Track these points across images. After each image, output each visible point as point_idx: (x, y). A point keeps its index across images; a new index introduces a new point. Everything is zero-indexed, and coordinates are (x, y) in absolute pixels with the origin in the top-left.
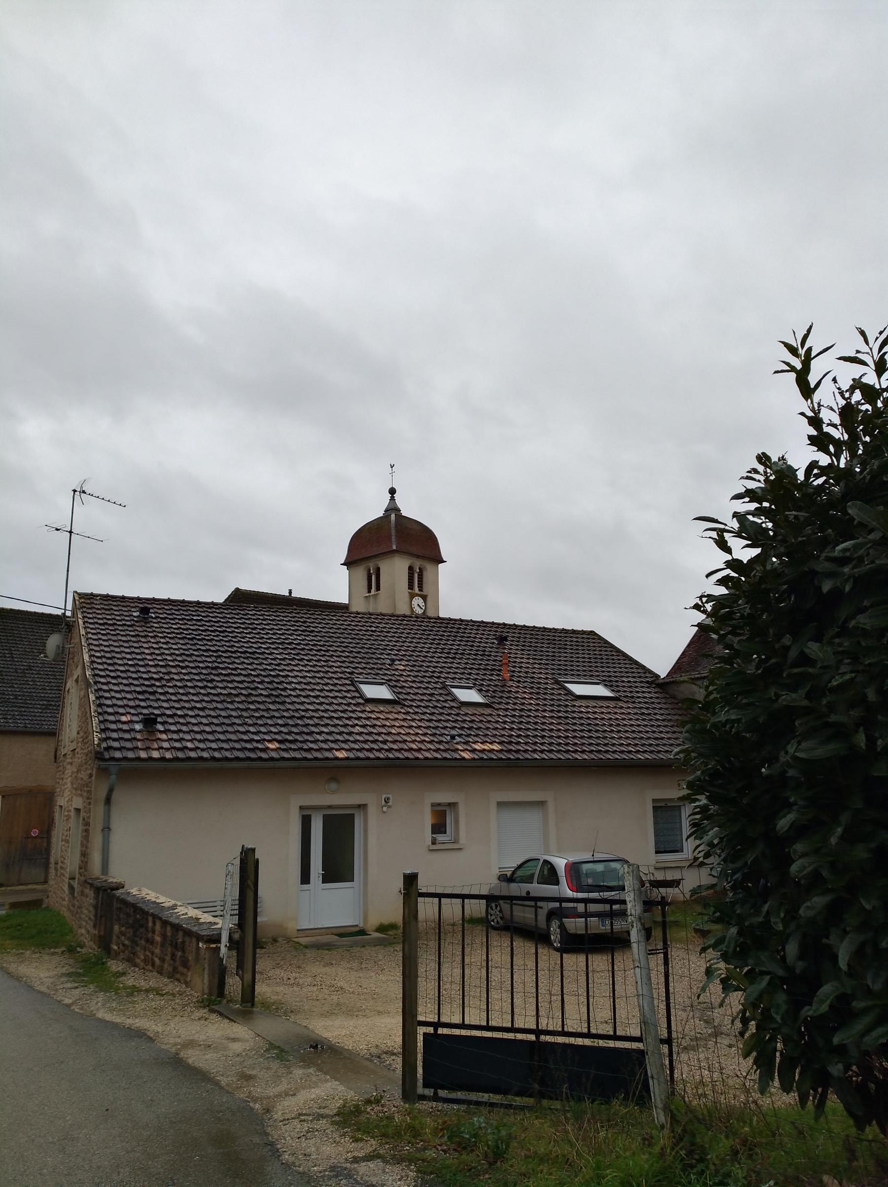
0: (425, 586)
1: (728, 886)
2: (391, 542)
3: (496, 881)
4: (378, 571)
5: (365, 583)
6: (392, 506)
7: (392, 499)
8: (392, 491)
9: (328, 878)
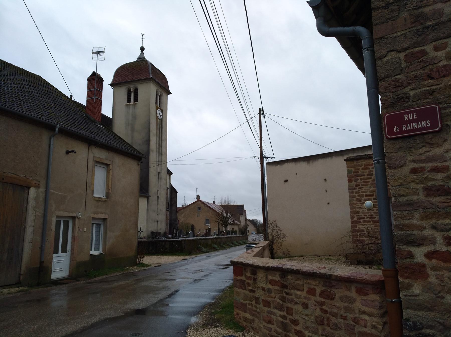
0: (161, 104)
1: (353, 171)
2: (149, 73)
3: (150, 233)
4: (136, 91)
5: (126, 97)
6: (141, 57)
7: (142, 53)
8: (142, 49)
9: (62, 252)
